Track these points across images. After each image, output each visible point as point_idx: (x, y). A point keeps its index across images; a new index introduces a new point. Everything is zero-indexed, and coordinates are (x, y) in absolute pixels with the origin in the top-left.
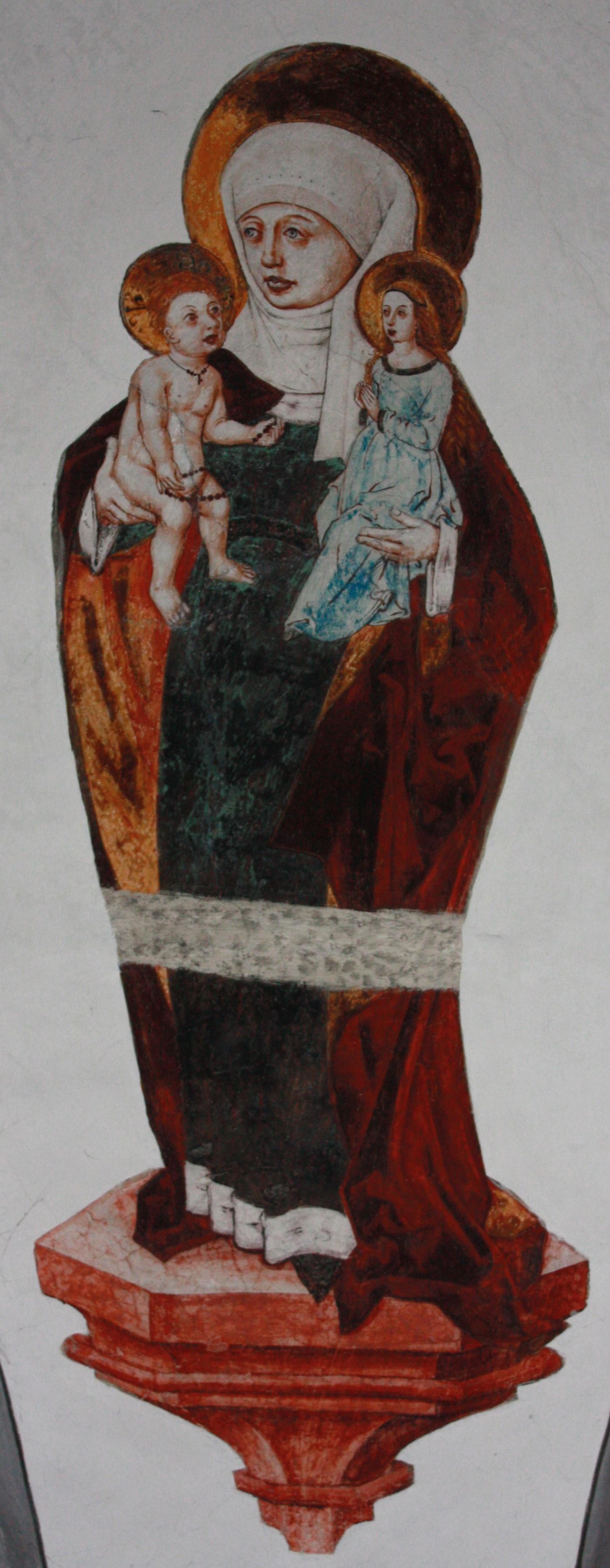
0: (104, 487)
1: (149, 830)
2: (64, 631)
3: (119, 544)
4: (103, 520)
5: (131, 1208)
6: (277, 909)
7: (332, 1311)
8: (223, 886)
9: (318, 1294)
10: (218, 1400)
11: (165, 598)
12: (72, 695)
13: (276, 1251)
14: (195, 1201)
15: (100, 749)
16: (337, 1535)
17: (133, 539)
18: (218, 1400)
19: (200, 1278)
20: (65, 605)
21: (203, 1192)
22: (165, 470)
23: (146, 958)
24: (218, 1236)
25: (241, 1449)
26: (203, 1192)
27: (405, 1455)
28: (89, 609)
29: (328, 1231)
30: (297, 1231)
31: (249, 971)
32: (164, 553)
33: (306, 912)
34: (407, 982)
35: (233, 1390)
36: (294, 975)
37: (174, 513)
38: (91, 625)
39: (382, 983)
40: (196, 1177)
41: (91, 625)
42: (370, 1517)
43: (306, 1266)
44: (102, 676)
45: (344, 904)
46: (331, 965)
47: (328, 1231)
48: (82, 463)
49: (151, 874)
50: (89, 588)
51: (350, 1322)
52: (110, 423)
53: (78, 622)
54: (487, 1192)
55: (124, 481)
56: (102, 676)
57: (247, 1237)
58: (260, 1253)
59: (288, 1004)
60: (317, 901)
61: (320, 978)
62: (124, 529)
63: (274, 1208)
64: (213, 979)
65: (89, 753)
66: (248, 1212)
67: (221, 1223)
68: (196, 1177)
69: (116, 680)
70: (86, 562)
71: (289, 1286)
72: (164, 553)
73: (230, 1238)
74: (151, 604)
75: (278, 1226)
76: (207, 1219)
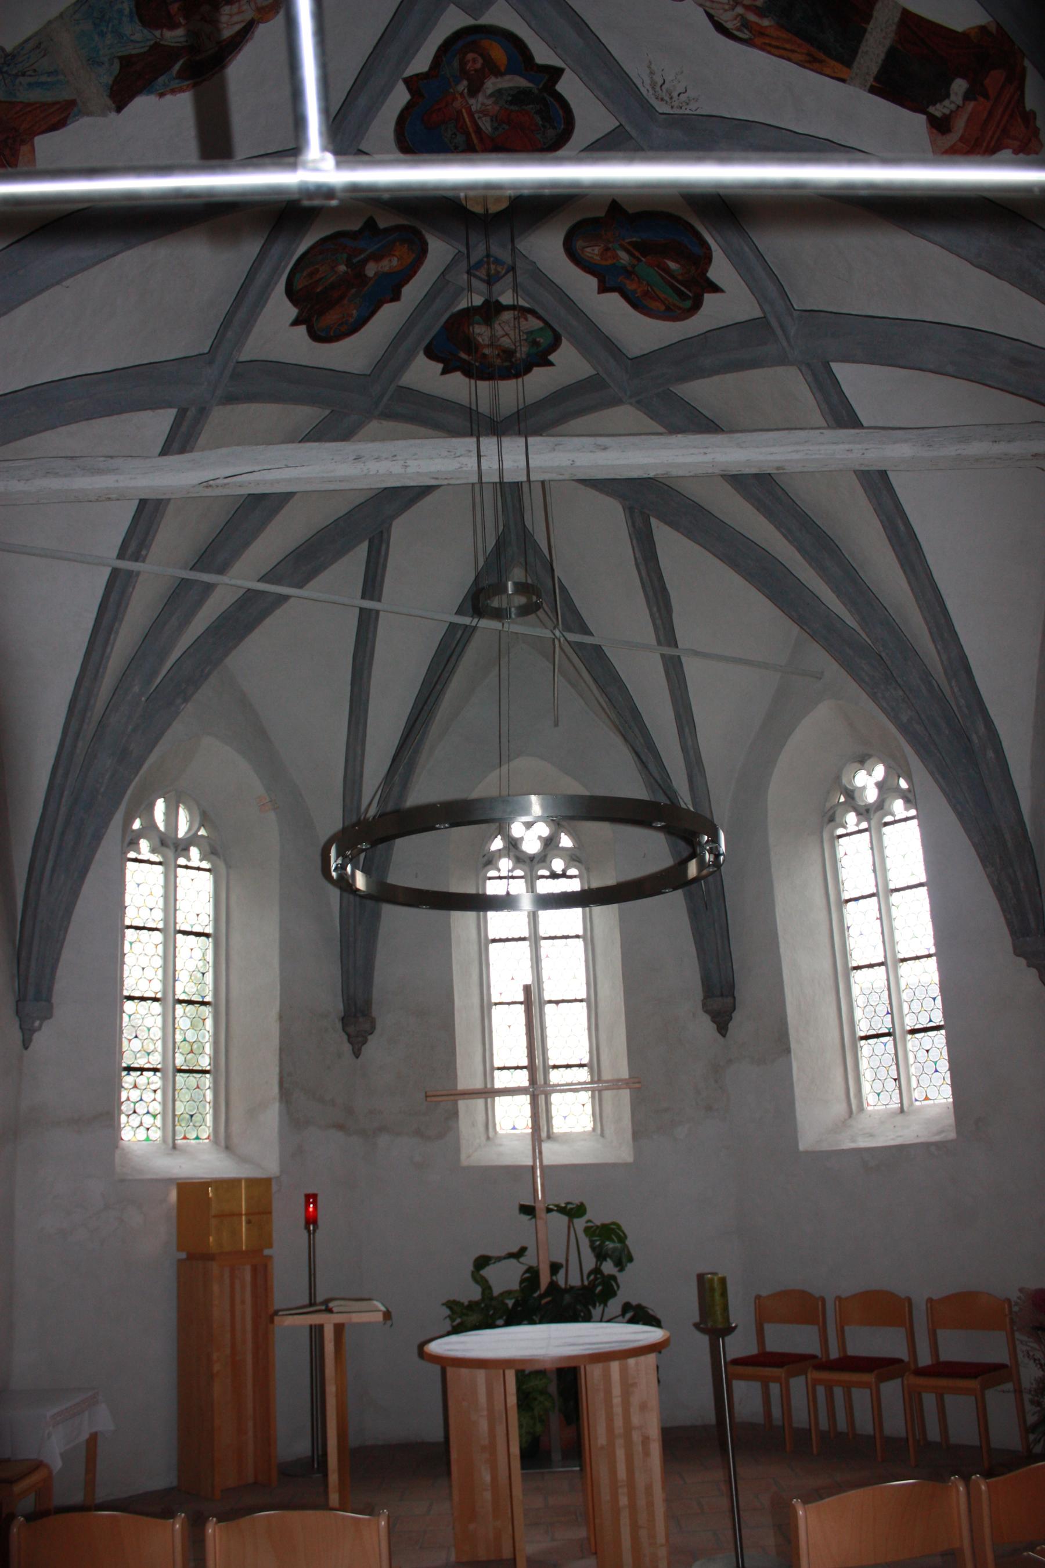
0: (729, 25)
1: (833, 63)
2: (769, 52)
3: (747, 28)
4: (738, 30)
5: (935, 131)
6: (864, 43)
7: (982, 99)
8: (854, 53)
9: (975, 99)
10: (993, 144)
11: (766, 22)
12: (789, 60)
13: (960, 102)
14: (938, 114)
15: (806, 62)
16: (1039, 141)
17: (745, 24)
18: (993, 144)
19: (960, 125)
20: (763, 50)
21: (938, 110)
22: (727, 7)
23: (868, 85)
24: (950, 115)
25: (1007, 147)
26: (938, 110)
27: (1028, 109)
28: (765, 44)
29: (959, 86)
30: (956, 94)
31: (880, 62)
32: (752, 17)
33: (867, 35)
34: (896, 20)
35: (992, 138)
36: (885, 50)
37: (740, 10)
38: (770, 45)
39: (894, 27)
40: (931, 110)
41: (770, 45)
42: (1029, 966)
43: (968, 97)
44: (785, 49)
45: (868, 22)
46: (884, 38)
47: (959, 86)
48: (720, 28)
49: (845, 69)
50: (759, 41)
51: (986, 96)
52: (710, 17)
53: (769, 48)
54: (964, 34)
55: (728, 19)
56: (785, 49)
57: (953, 107)
58: (958, 107)
59: (892, 54)
60: (865, 30)
61: (888, 43)
62: (743, 25)
63: (948, 96)
64: (879, 72)
65: (807, 65)
66: (946, 103)
67: (947, 112)
68: (931, 110)
69: (787, 46)
70: (751, 39)
71: (971, 105)
72: (752, 17)
73: (952, 112)
74: (766, 27)
75: (953, 97)
76: (944, 114)
